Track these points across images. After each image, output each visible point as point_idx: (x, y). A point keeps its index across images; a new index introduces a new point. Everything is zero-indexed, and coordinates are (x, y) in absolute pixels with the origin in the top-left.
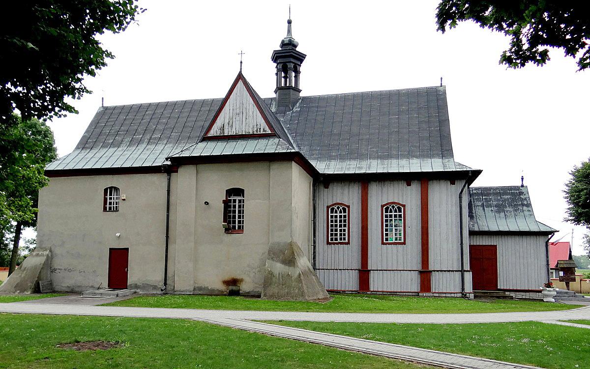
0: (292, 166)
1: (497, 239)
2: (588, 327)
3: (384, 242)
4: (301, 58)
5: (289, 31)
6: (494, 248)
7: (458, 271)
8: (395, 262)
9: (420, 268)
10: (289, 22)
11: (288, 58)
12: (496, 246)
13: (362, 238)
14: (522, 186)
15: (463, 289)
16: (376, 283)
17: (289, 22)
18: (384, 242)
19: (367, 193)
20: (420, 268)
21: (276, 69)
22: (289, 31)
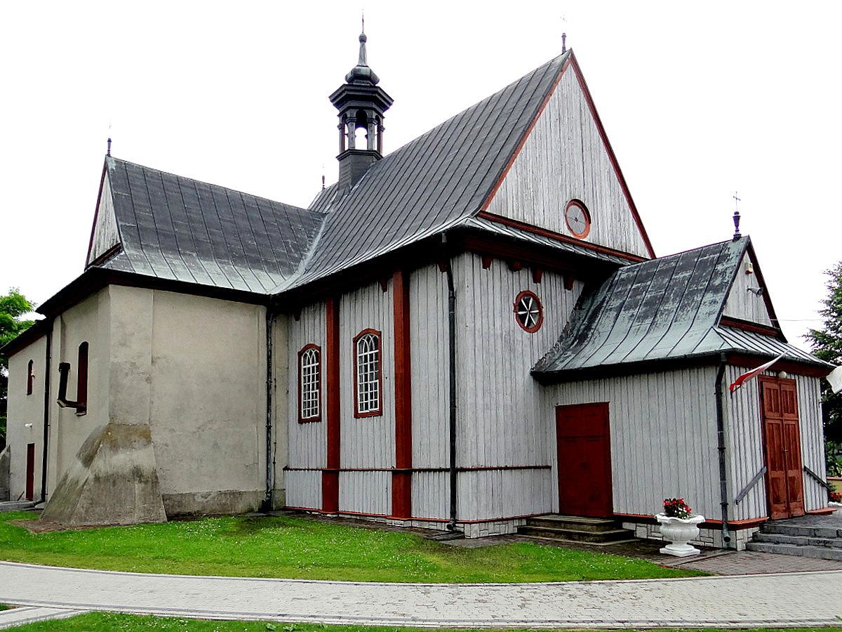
0: (109, 295)
1: (687, 385)
2: (1, 612)
3: (359, 412)
4: (340, 99)
5: (362, 57)
6: (604, 407)
7: (345, 470)
8: (371, 460)
9: (325, 466)
10: (363, 39)
11: (361, 100)
12: (607, 404)
13: (717, 405)
14: (737, 237)
15: (453, 513)
16: (347, 503)
17: (363, 39)
18: (359, 412)
19: (65, 335)
20: (325, 466)
21: (385, 123)
22: (362, 57)
